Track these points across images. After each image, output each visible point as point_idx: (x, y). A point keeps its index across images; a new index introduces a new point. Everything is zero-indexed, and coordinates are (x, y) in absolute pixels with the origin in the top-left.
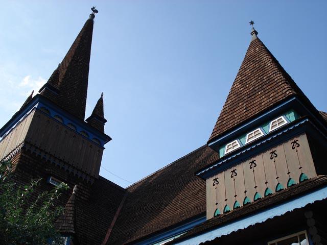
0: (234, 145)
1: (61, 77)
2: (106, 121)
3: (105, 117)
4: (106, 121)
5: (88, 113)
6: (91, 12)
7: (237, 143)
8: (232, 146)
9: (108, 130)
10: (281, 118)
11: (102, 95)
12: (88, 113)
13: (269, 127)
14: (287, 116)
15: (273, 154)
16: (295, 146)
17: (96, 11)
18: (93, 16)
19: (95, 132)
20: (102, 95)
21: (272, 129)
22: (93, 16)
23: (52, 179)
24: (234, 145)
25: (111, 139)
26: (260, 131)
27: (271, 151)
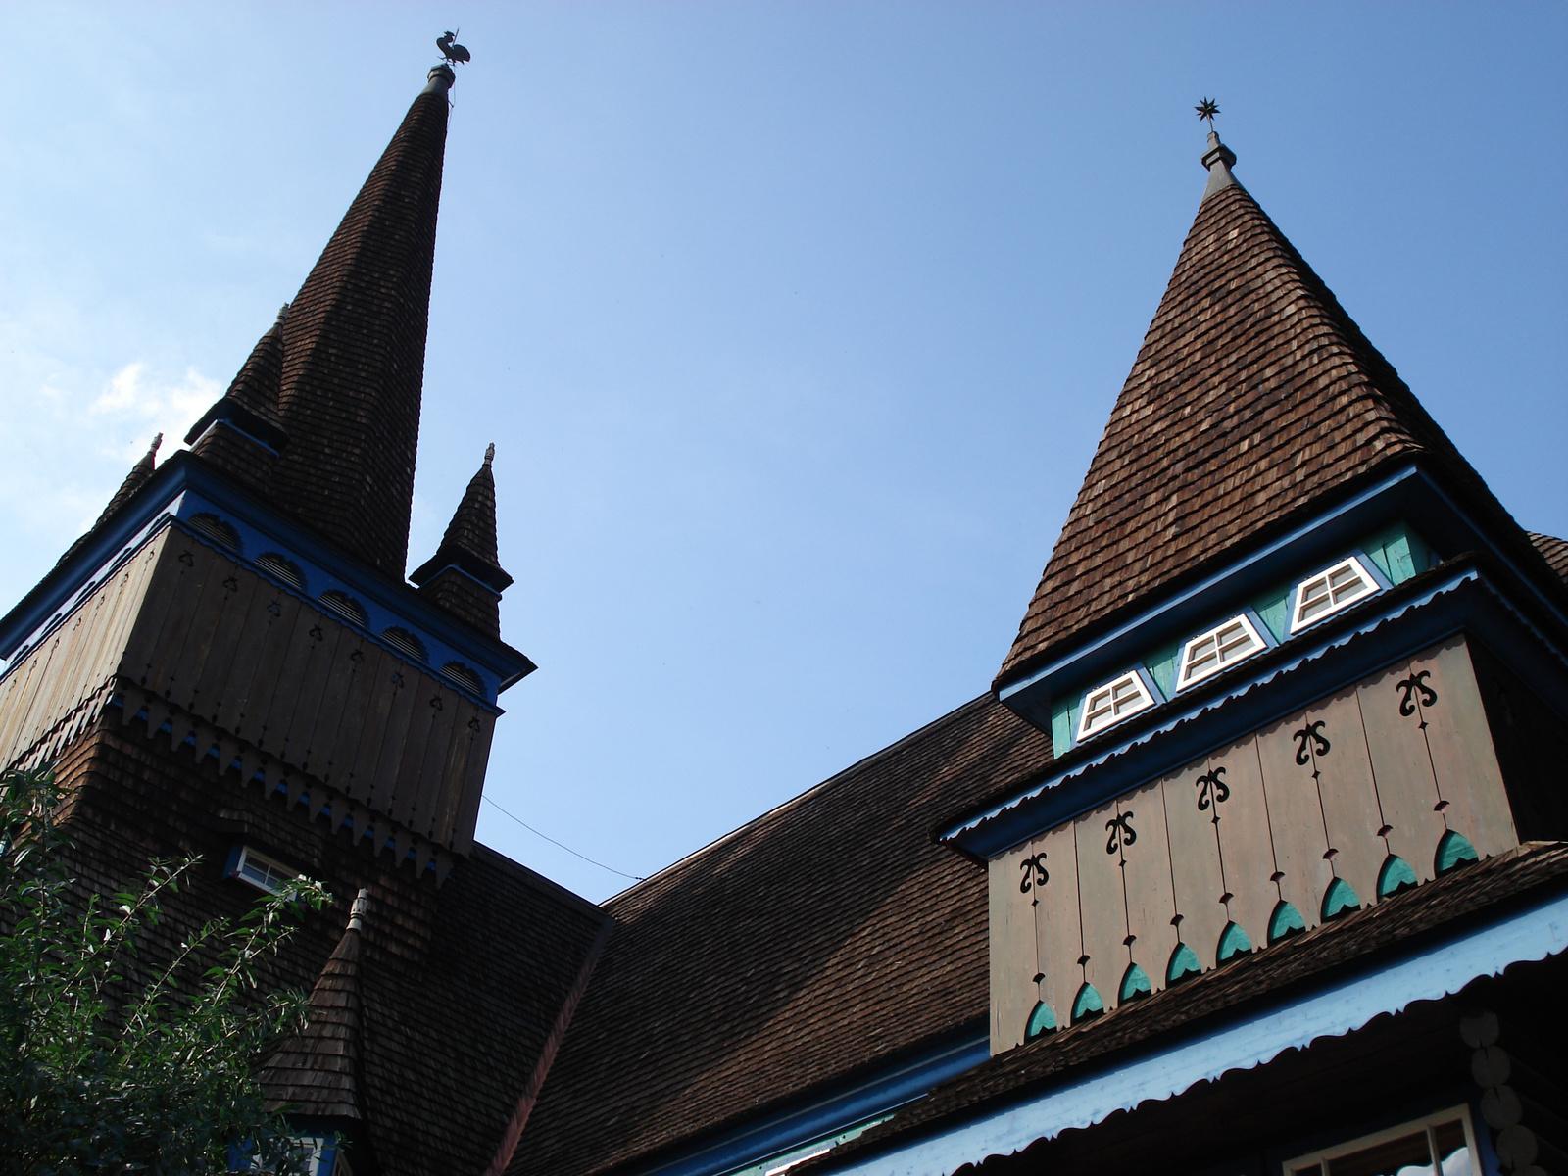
0: (1123, 694)
1: (293, 370)
2: (507, 581)
3: (506, 560)
4: (507, 581)
5: (423, 543)
6: (438, 58)
7: (1138, 685)
8: (1110, 701)
9: (517, 622)
10: (1238, 626)
11: (489, 457)
12: (423, 543)
13: (1289, 608)
14: (1378, 555)
15: (1415, 690)
16: (1208, 797)
17: (461, 54)
18: (444, 78)
19: (455, 635)
20: (489, 457)
21: (1302, 617)
22: (444, 78)
23: (249, 860)
24: (1123, 694)
25: (537, 668)
26: (1248, 629)
27: (1111, 814)
